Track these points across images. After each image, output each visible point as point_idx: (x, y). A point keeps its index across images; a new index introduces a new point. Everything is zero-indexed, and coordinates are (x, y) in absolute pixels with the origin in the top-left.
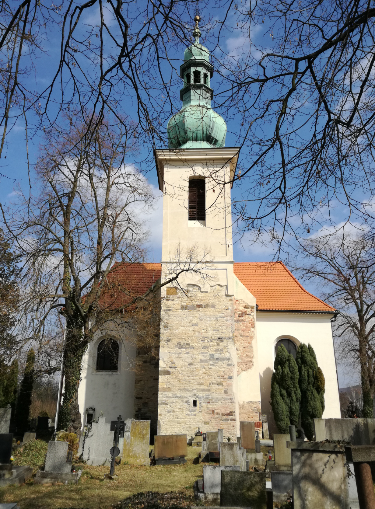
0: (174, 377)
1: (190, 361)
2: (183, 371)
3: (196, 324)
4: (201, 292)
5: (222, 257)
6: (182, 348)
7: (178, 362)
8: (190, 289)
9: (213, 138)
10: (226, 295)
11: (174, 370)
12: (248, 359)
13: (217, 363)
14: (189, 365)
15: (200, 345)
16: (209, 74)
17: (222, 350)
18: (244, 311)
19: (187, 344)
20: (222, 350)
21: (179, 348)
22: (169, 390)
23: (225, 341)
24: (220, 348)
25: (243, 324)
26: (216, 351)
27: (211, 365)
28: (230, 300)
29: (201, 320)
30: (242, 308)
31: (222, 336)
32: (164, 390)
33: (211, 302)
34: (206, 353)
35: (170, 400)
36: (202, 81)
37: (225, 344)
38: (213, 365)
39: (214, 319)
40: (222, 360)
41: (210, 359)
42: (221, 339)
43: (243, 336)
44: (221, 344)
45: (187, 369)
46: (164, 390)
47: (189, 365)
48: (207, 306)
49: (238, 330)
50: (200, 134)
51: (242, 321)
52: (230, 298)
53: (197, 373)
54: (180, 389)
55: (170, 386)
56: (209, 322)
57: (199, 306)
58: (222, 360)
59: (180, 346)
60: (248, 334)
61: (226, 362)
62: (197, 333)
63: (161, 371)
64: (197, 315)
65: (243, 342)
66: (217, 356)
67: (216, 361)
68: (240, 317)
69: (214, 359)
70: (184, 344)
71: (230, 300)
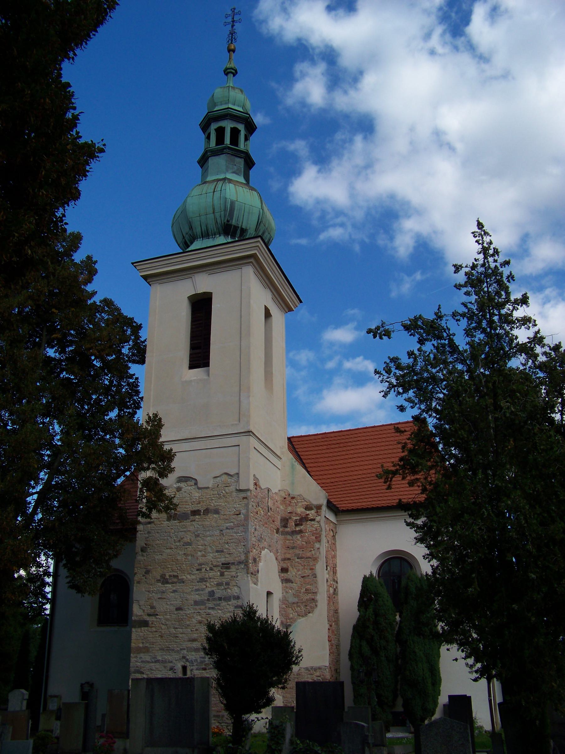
0: (154, 629)
1: (178, 603)
2: (167, 620)
3: (189, 544)
4: (199, 488)
5: (233, 425)
6: (168, 583)
7: (161, 607)
8: (182, 485)
9: (236, 228)
10: (237, 490)
11: (153, 618)
12: (310, 596)
13: (219, 605)
14: (177, 609)
15: (194, 577)
16: (241, 127)
17: (228, 584)
18: (304, 515)
19: (175, 576)
20: (228, 584)
21: (163, 583)
22: (146, 650)
23: (233, 568)
24: (224, 581)
25: (302, 537)
26: (219, 584)
27: (210, 608)
28: (244, 498)
29: (198, 536)
30: (300, 510)
31: (229, 559)
32: (139, 650)
33: (213, 504)
34: (203, 590)
35: (148, 666)
36: (227, 140)
37: (234, 574)
38: (213, 608)
39: (217, 533)
40: (227, 599)
41: (208, 600)
42: (226, 566)
43: (301, 558)
44: (226, 573)
45: (174, 616)
46: (139, 650)
47: (177, 609)
48: (207, 511)
49: (293, 548)
50: (212, 226)
51: (301, 531)
52: (243, 495)
53: (188, 623)
54: (162, 649)
55: (147, 645)
56: (209, 538)
57: (195, 513)
58: (227, 599)
59: (164, 580)
60: (309, 554)
61: (233, 602)
62: (190, 558)
63: (135, 621)
64: (192, 528)
65: (301, 568)
66: (219, 593)
67: (218, 602)
68: (296, 525)
69: (214, 600)
70: (170, 576)
71: (244, 498)
